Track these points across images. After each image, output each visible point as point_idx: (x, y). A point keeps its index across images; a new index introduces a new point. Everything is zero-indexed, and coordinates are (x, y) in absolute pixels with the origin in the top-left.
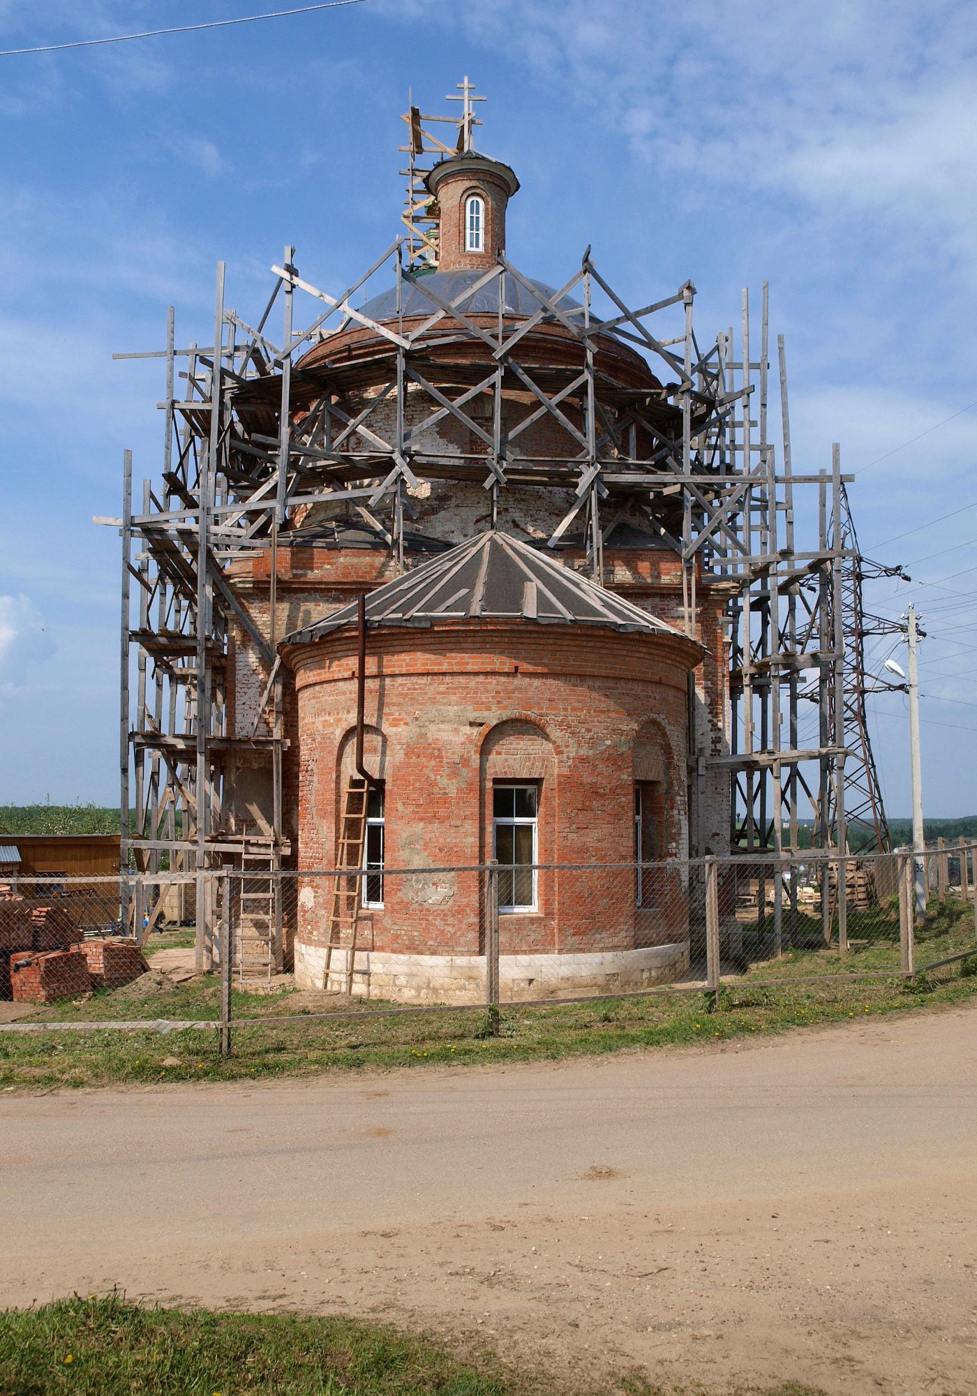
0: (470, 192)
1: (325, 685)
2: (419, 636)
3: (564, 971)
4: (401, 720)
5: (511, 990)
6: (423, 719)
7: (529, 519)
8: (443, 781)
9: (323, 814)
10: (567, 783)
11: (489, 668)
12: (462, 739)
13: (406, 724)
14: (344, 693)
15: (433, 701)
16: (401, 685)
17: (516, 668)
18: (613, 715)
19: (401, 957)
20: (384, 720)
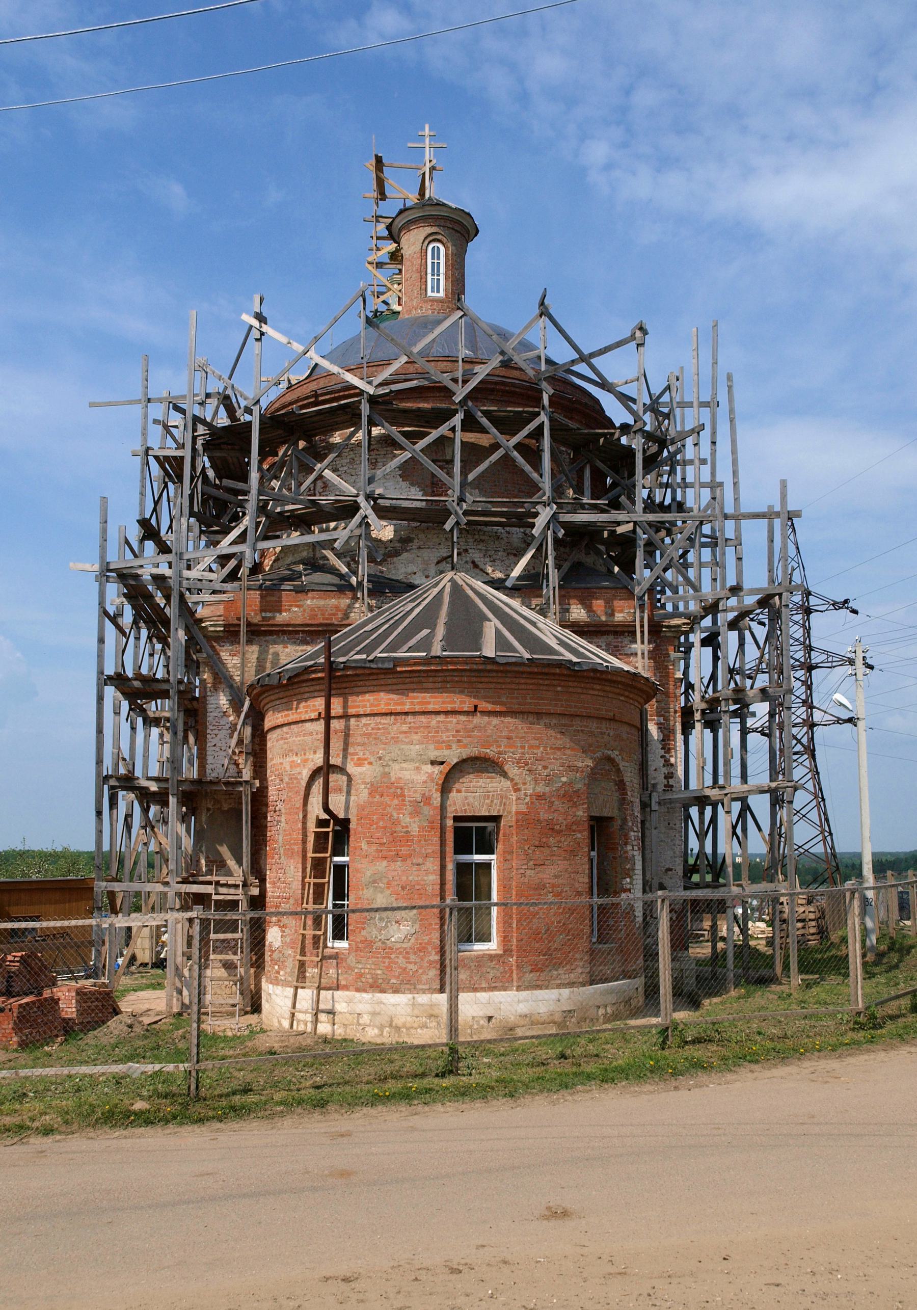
0: (431, 238)
1: (292, 726)
2: (383, 676)
3: (523, 1008)
4: (365, 759)
5: (471, 1027)
6: (387, 758)
7: (487, 560)
8: (406, 820)
9: (290, 854)
10: (525, 820)
11: (449, 707)
12: (424, 778)
13: (370, 763)
14: (311, 734)
15: (396, 740)
16: (365, 725)
17: (476, 707)
18: (568, 752)
19: (364, 995)
20: (349, 760)
